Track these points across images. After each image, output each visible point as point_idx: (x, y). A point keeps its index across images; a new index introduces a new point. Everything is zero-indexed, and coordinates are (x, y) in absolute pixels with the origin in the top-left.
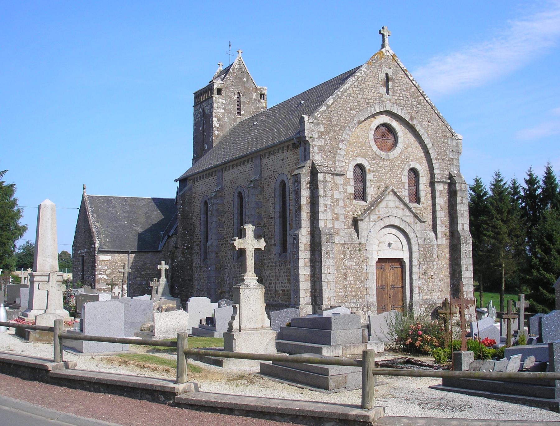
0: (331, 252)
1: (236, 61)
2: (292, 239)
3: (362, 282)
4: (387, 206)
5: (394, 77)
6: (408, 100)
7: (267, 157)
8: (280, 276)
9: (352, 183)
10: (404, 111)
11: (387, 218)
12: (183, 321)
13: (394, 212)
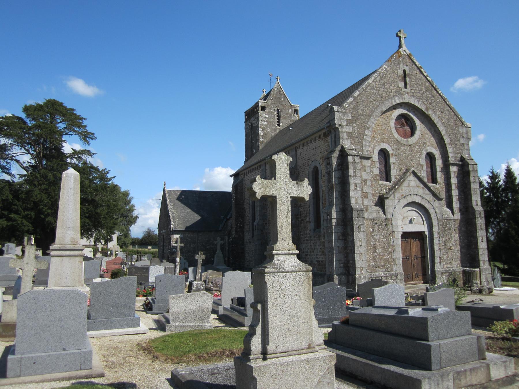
0: (362, 226)
1: (276, 86)
2: (325, 215)
3: (390, 253)
6: (423, 93)
7: (301, 148)
8: (315, 249)
9: (377, 165)
10: (420, 103)
11: (409, 196)
12: (206, 305)
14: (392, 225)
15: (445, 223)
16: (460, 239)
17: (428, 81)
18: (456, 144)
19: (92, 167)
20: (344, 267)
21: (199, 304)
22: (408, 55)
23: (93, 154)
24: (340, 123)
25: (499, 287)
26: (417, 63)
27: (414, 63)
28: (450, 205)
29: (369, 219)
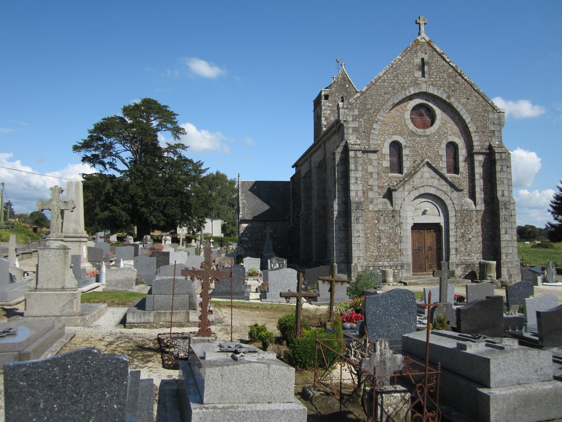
0: (360, 218)
3: (396, 244)
4: (422, 177)
5: (430, 61)
6: (445, 81)
9: (388, 158)
12: (131, 276)
13: (430, 182)
14: (400, 216)
15: (464, 215)
16: (483, 230)
17: (452, 67)
18: (484, 132)
19: (186, 160)
20: (344, 256)
21: (126, 275)
22: (427, 42)
23: (186, 147)
24: (345, 119)
25: (553, 282)
26: (438, 49)
27: (435, 49)
28: (472, 196)
29: (374, 211)
